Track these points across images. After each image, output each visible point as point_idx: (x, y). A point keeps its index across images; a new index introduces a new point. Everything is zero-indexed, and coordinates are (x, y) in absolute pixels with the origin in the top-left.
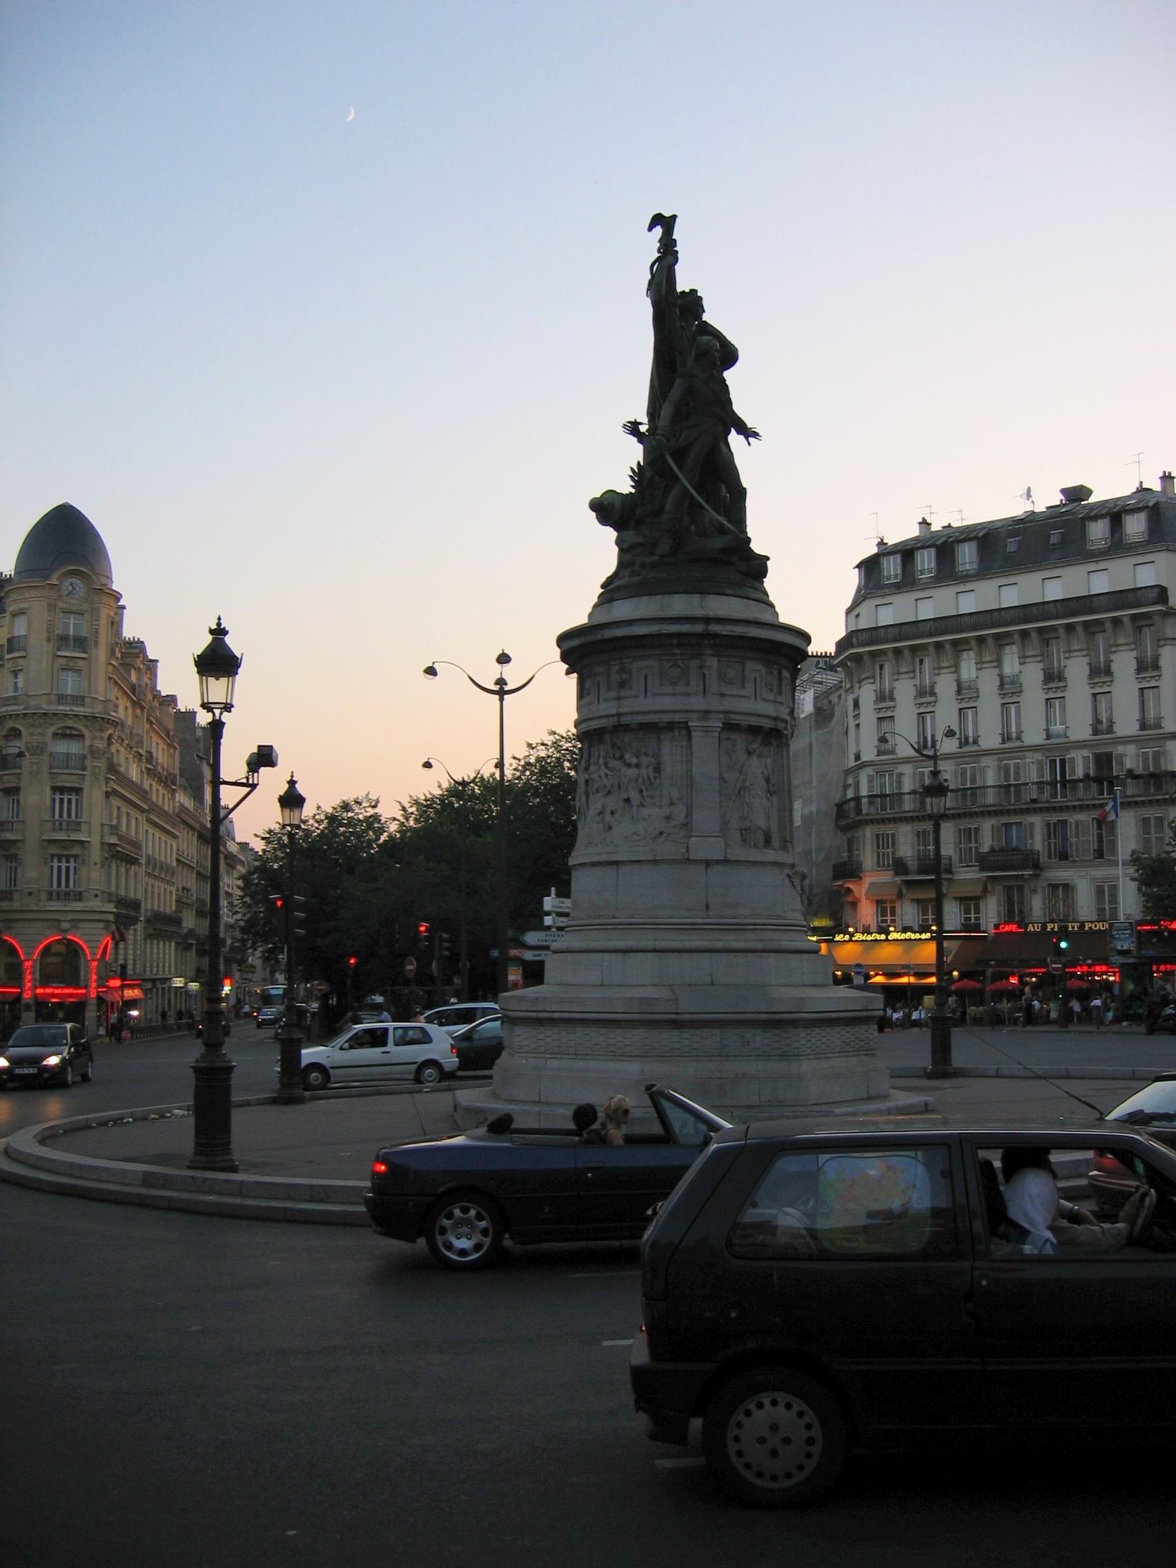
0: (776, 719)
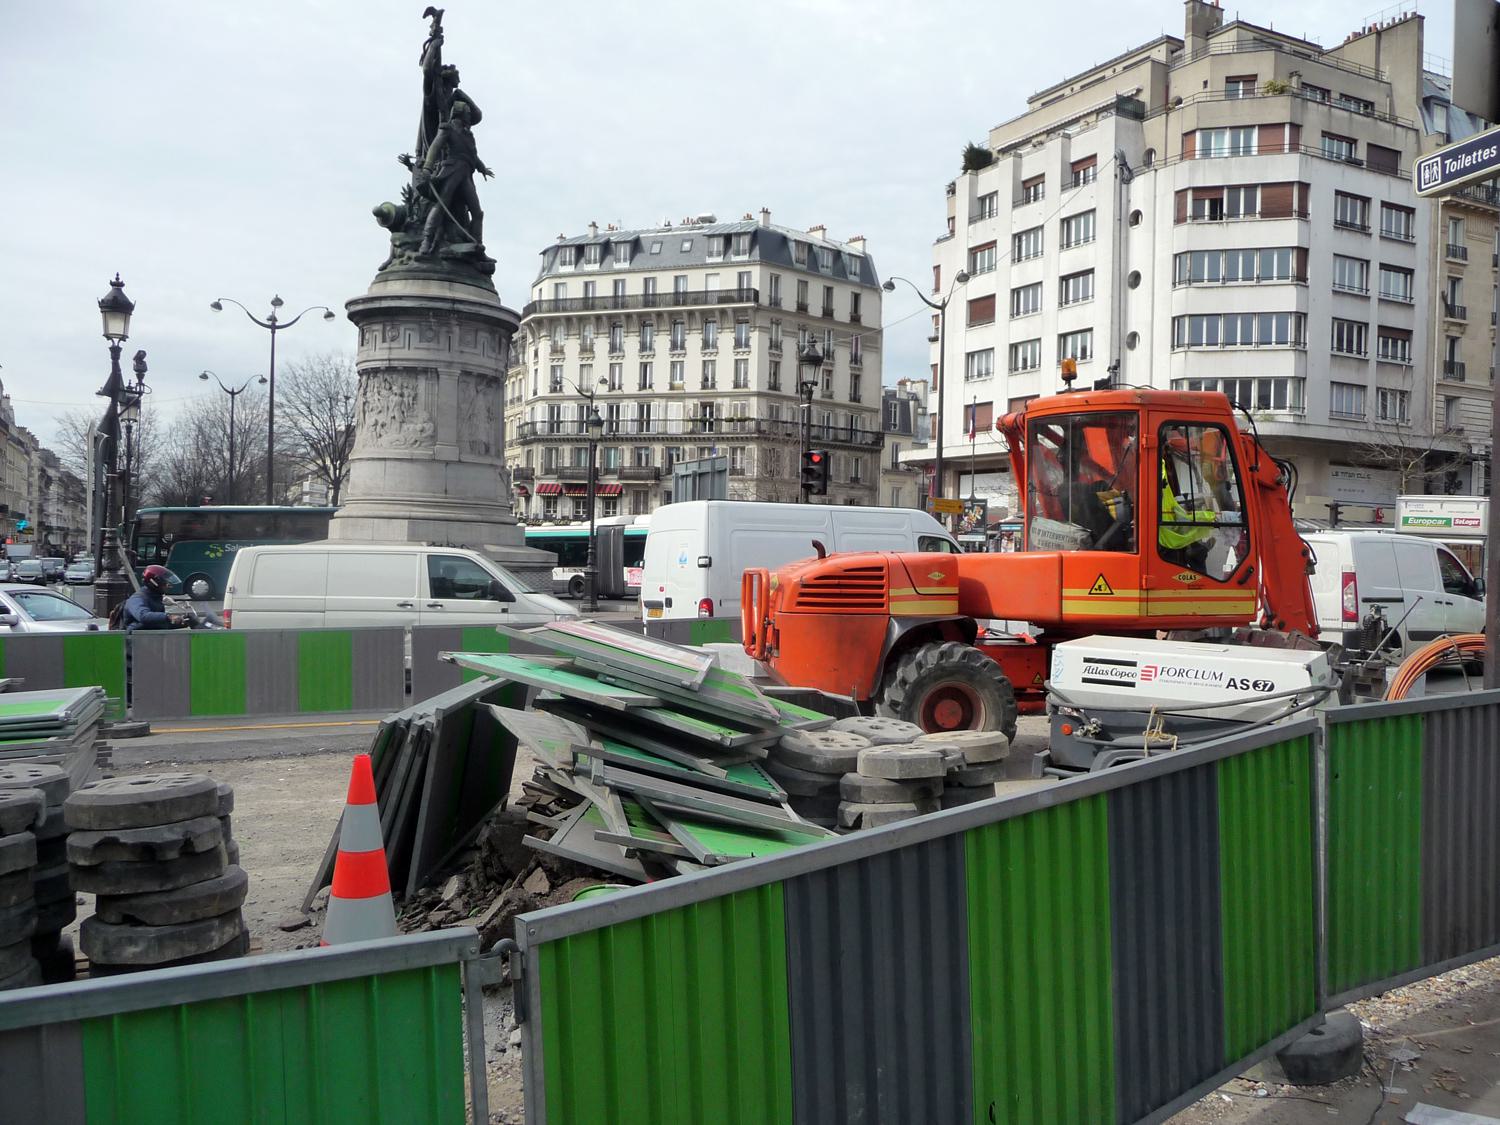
0: (496, 370)
